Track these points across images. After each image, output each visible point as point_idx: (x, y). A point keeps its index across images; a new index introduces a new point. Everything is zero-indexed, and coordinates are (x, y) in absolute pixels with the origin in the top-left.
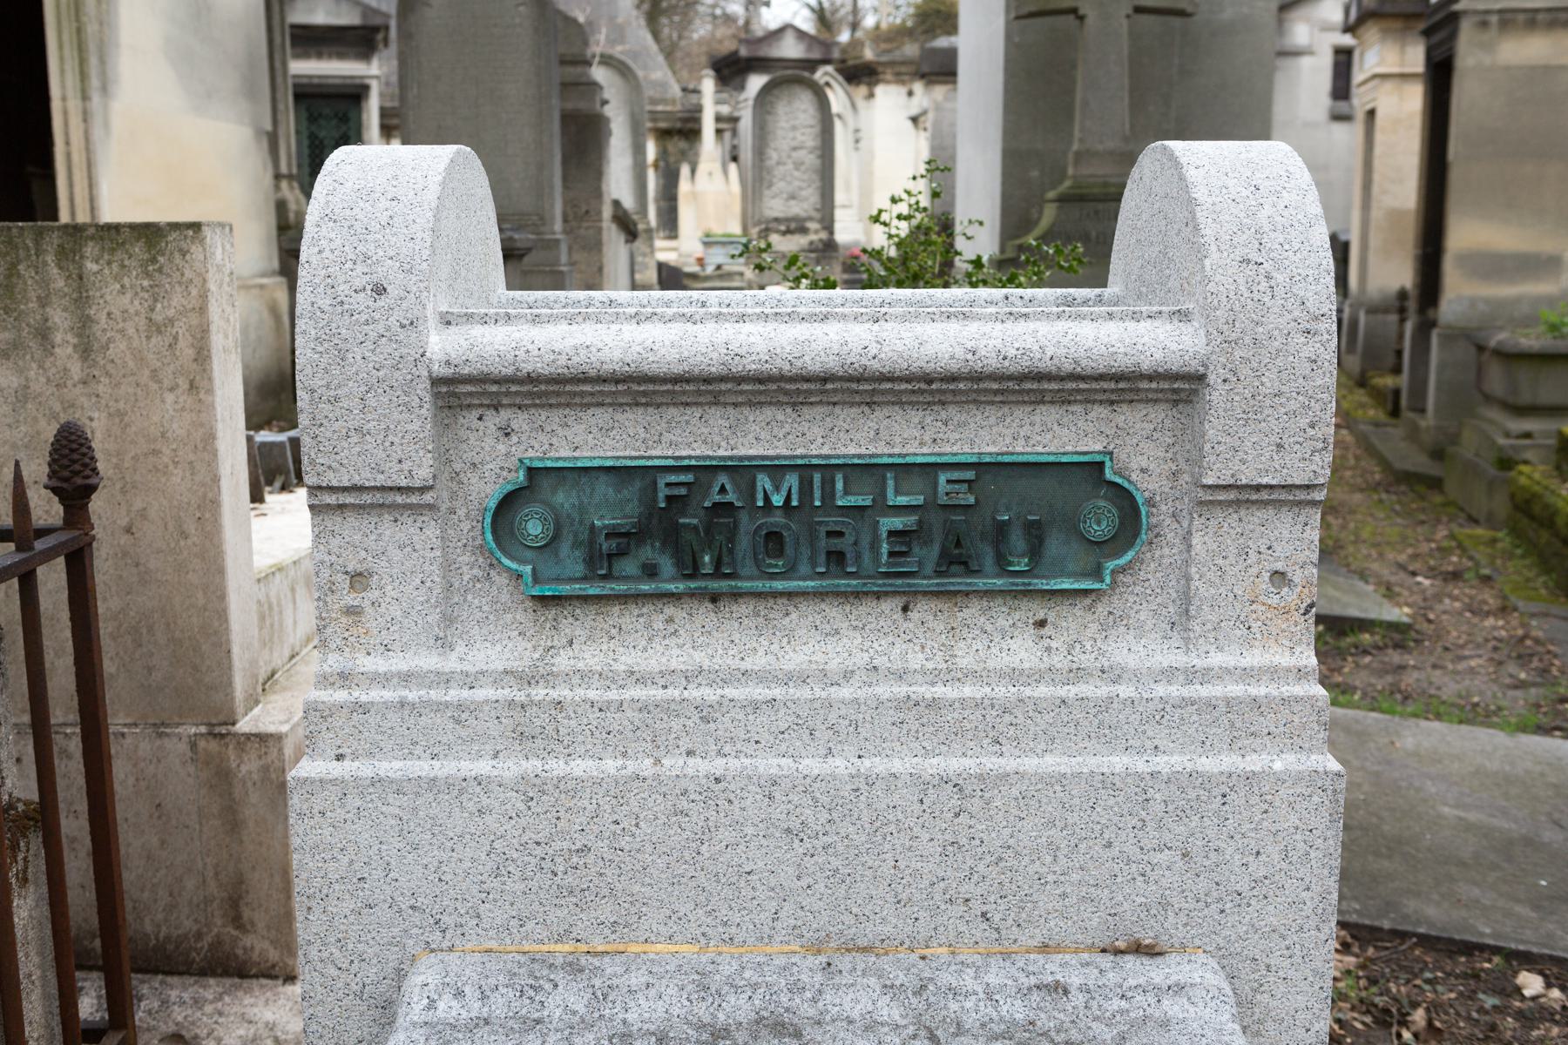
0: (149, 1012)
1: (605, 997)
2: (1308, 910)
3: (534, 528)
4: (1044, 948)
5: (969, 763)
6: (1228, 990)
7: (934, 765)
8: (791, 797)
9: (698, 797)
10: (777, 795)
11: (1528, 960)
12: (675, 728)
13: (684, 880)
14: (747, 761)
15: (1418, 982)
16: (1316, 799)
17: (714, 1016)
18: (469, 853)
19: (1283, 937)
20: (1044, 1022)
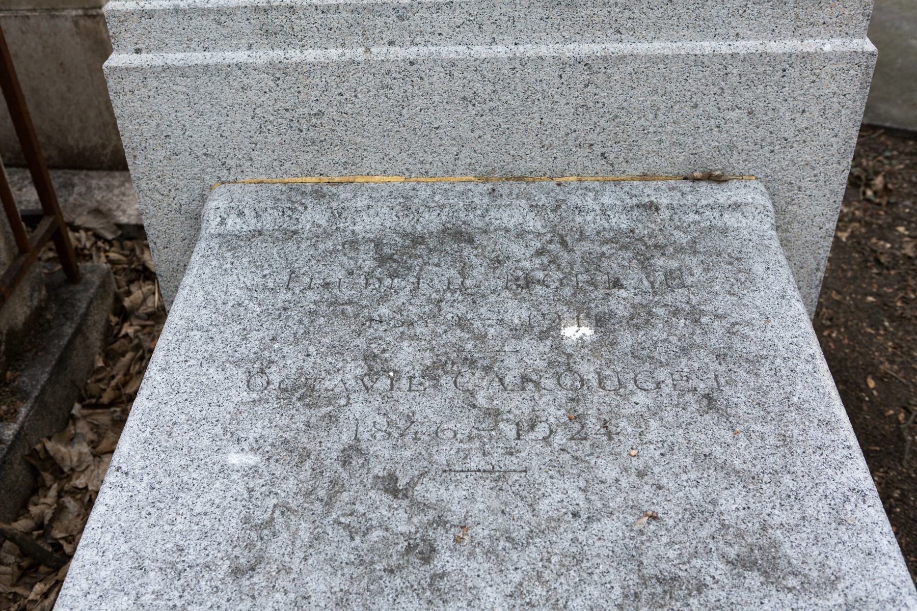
0: (80, 194)
1: (340, 215)
2: (833, 150)
4: (644, 177)
5: (597, 48)
6: (771, 208)
7: (571, 50)
8: (466, 74)
9: (398, 76)
10: (455, 73)
12: (379, 25)
13: (392, 133)
14: (433, 49)
15: (881, 158)
16: (852, 72)
17: (414, 227)
18: (239, 117)
19: (813, 168)
20: (641, 231)
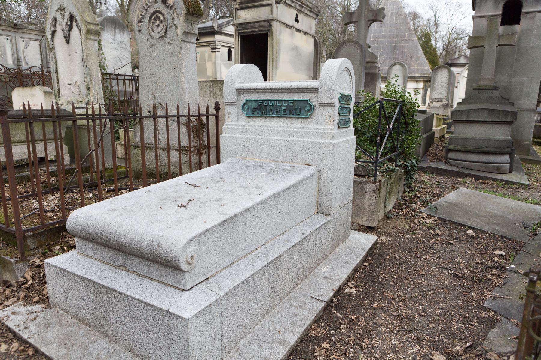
3: (246, 108)
5: (290, 139)
11: (470, 228)
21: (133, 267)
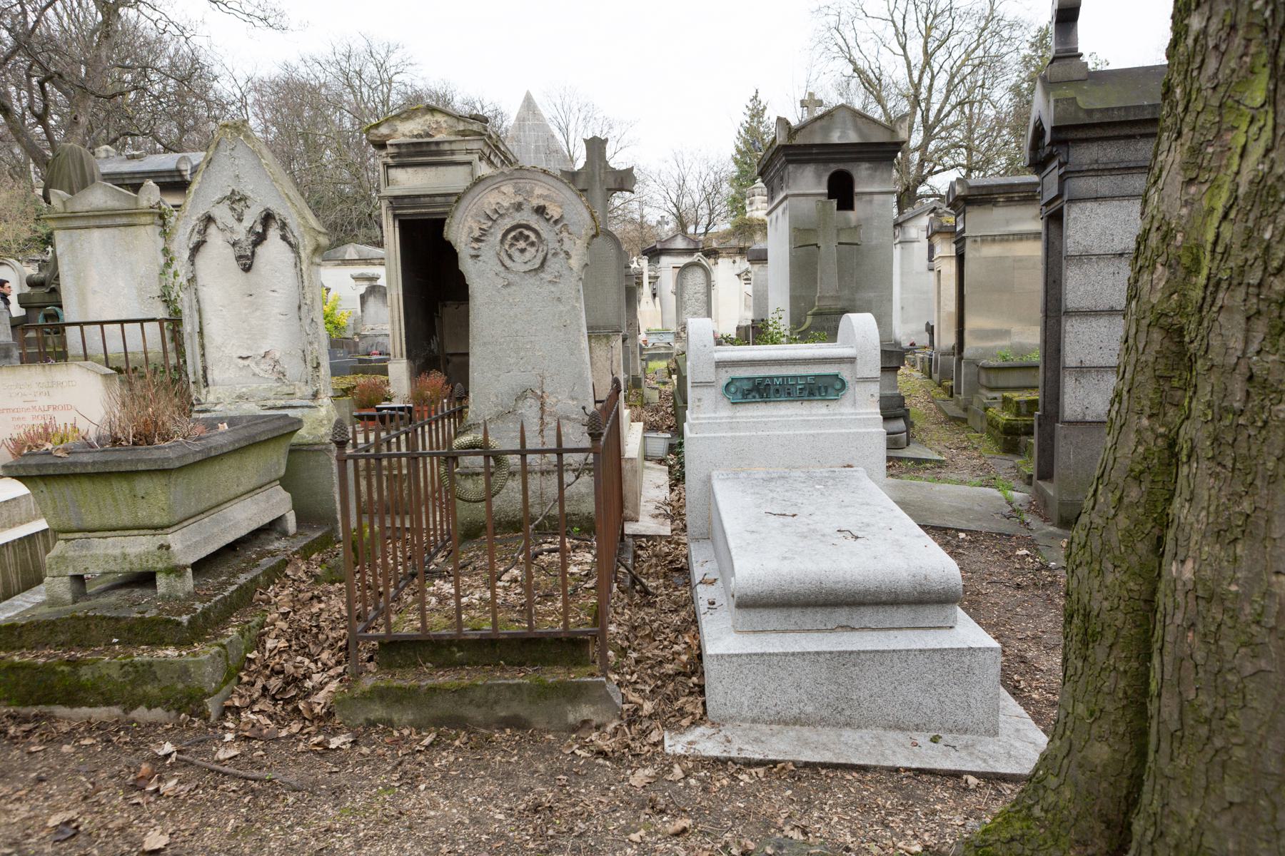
3: (733, 390)
21: (866, 621)
